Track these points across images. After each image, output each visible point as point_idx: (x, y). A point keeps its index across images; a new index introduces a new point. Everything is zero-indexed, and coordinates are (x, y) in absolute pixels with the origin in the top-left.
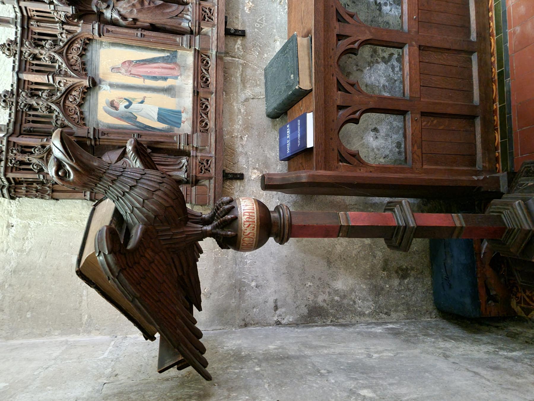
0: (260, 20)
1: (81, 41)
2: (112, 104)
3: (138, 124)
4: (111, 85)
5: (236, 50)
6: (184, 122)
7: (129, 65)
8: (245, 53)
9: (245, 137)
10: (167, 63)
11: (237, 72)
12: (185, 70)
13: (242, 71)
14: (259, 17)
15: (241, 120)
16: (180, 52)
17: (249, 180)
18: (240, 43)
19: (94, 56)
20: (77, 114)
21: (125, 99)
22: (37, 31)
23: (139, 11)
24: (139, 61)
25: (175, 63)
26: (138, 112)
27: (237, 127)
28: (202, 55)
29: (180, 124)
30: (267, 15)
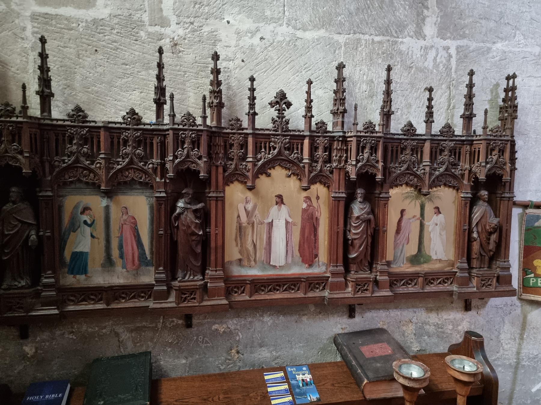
0: (206, 341)
1: (149, 180)
2: (86, 209)
3: (67, 233)
4: (107, 208)
5: (170, 319)
6: (74, 277)
7: (132, 223)
8: (169, 329)
9: (74, 336)
10: (139, 258)
11: (147, 322)
12: (134, 275)
13: (150, 327)
14: (210, 340)
15: (92, 330)
16: (152, 269)
17: (21, 344)
18: (179, 322)
19: (137, 191)
20: (70, 178)
21: (94, 221)
22: (154, 142)
23: (184, 231)
24: (138, 231)
25: (140, 265)
26: (81, 233)
27: (84, 328)
28: (150, 292)
29: (72, 273)
30: (213, 347)
